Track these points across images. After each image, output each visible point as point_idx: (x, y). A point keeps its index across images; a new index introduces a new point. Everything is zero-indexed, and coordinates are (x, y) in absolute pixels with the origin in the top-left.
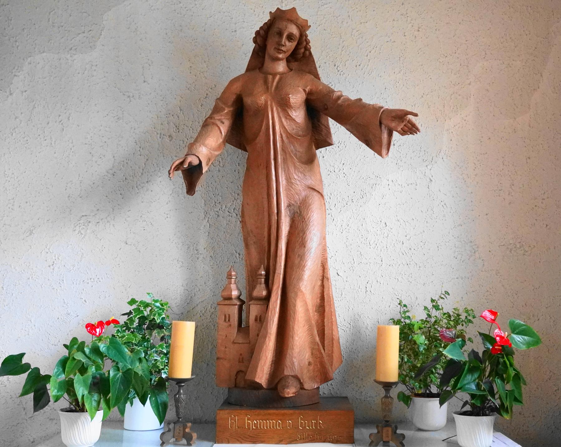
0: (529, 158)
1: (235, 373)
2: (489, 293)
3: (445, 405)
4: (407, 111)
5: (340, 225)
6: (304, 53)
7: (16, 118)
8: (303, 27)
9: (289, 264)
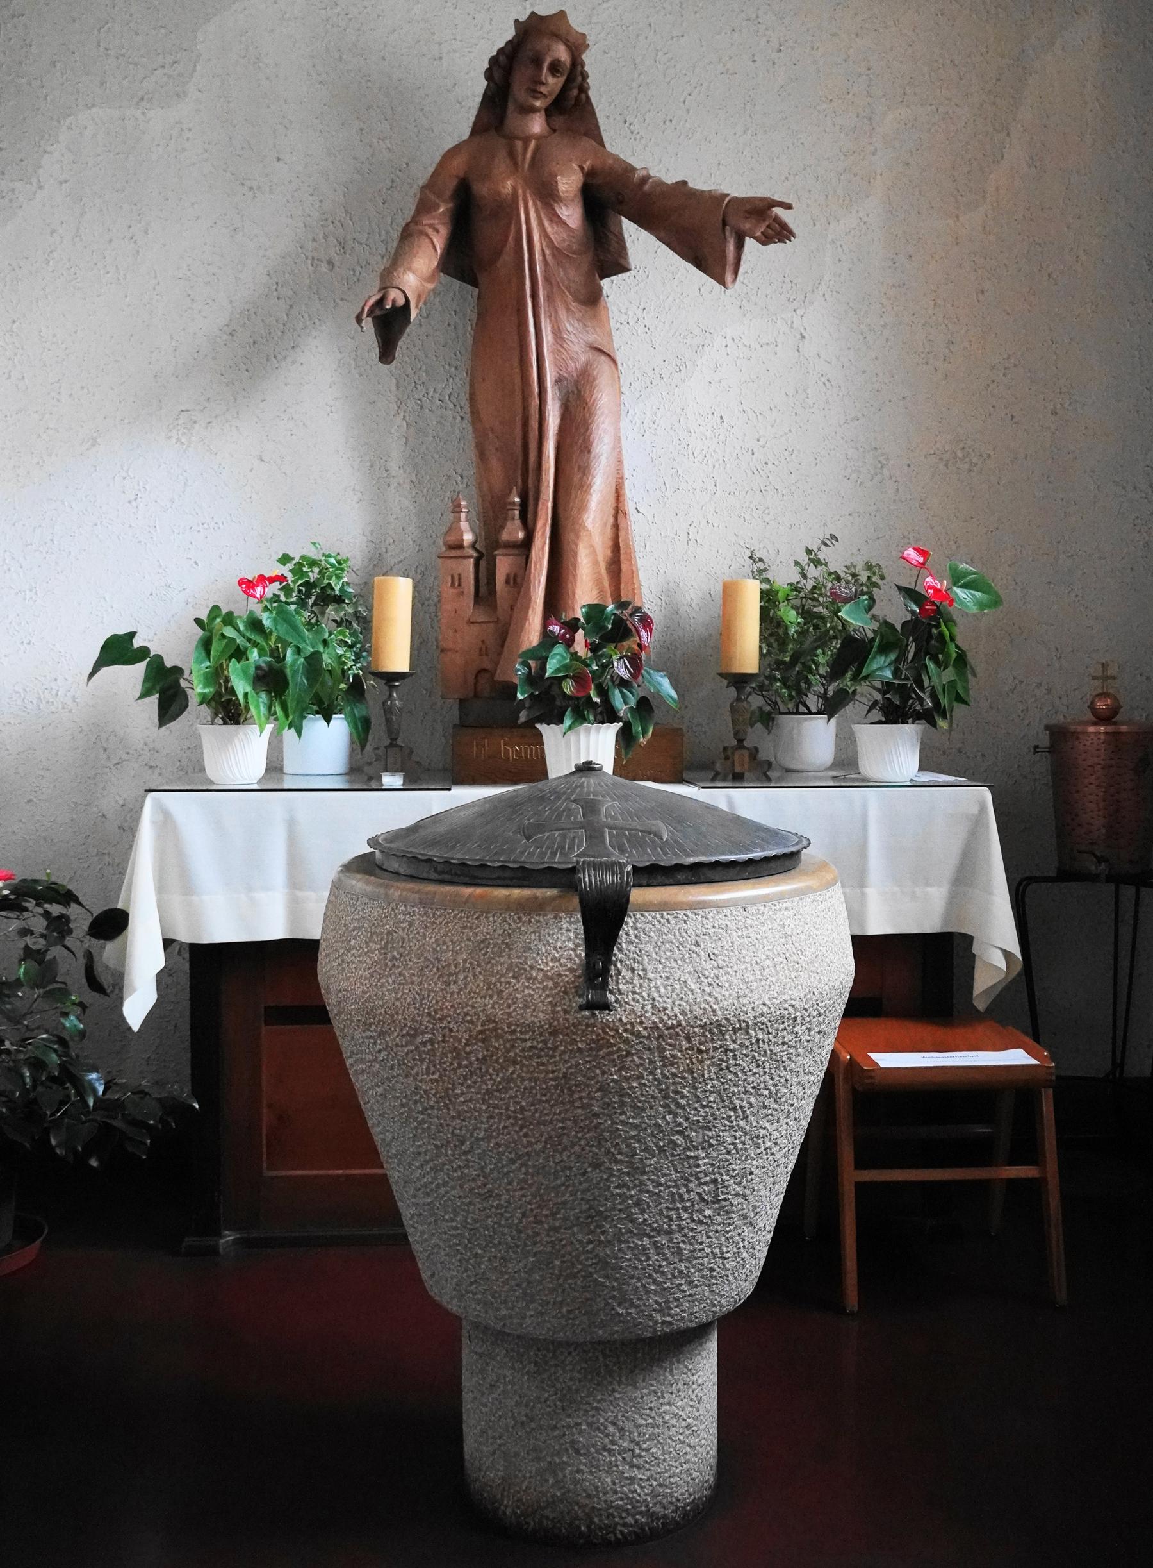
0: (983, 292)
1: (474, 673)
2: (906, 541)
3: (833, 721)
4: (773, 201)
5: (639, 422)
6: (577, 98)
7: (53, 232)
8: (577, 46)
9: (562, 483)
